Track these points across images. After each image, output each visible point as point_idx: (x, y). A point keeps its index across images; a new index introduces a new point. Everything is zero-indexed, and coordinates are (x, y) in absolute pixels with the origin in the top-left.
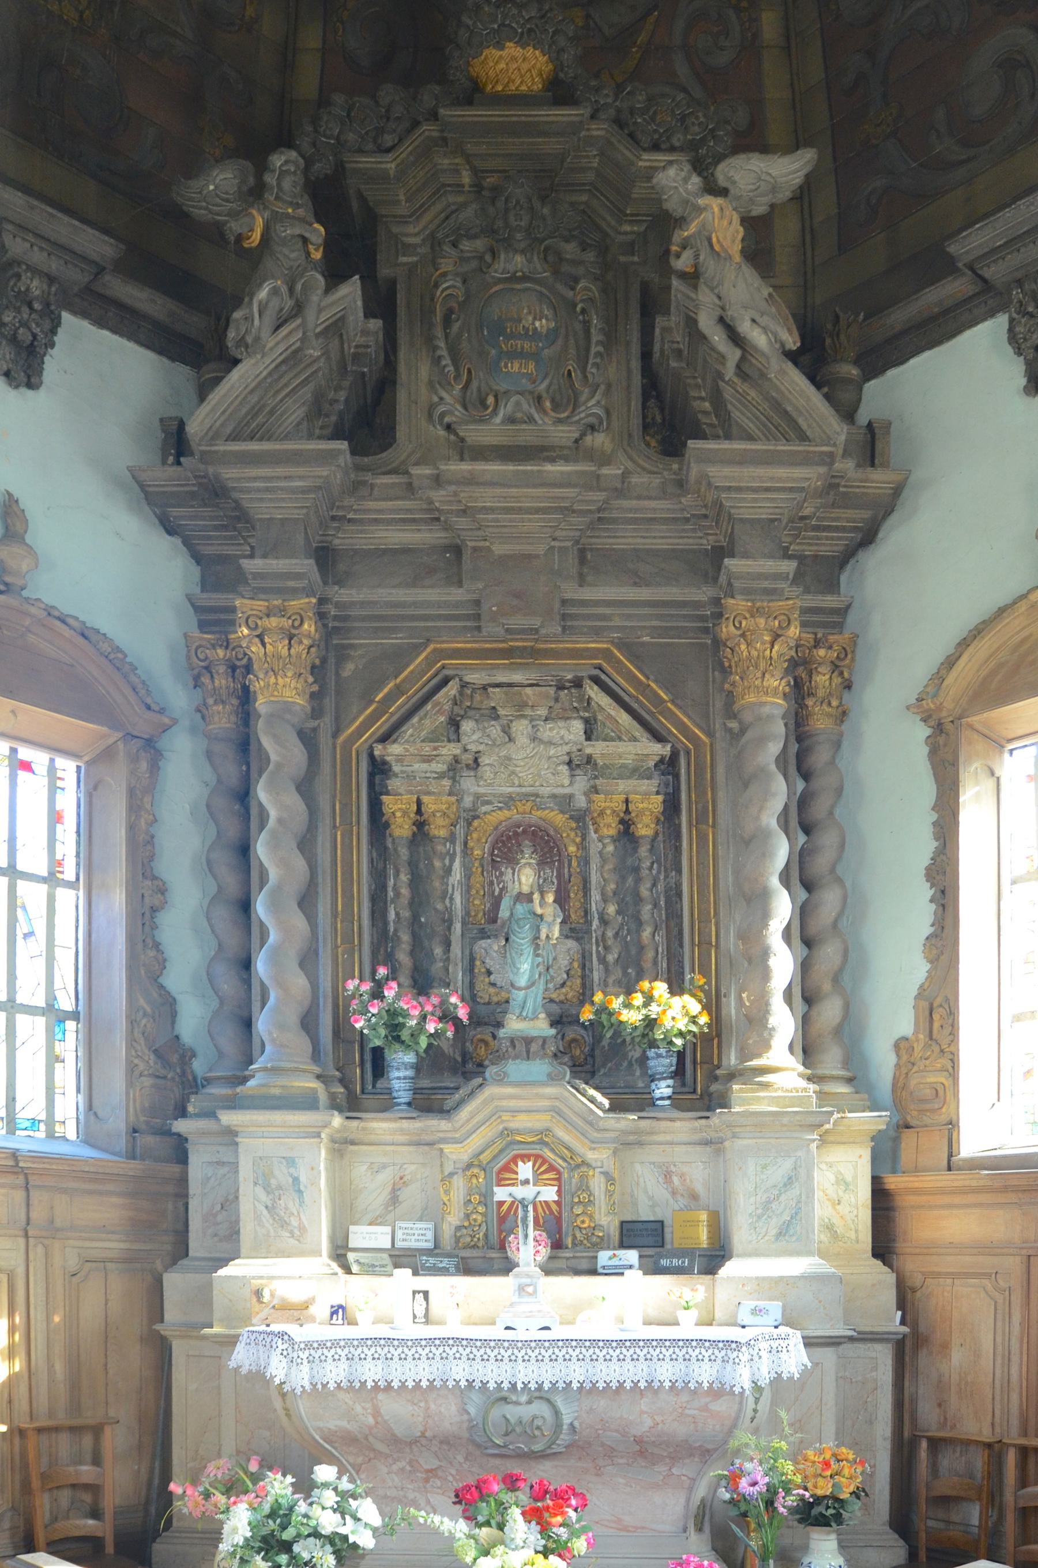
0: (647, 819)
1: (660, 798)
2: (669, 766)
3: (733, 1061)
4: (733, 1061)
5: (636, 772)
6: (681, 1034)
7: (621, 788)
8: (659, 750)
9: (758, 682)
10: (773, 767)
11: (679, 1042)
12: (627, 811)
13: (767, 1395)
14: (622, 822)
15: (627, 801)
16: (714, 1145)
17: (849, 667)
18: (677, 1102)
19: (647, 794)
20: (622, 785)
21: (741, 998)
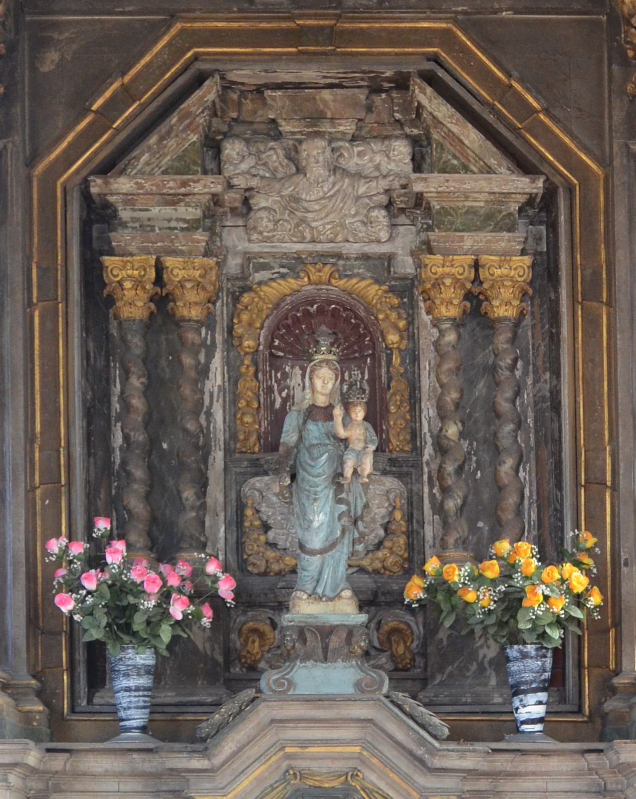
0: (506, 293)
1: (527, 260)
2: (542, 208)
5: (492, 219)
8: (525, 186)
12: (477, 280)
15: (476, 265)
19: (505, 254)
20: (470, 240)
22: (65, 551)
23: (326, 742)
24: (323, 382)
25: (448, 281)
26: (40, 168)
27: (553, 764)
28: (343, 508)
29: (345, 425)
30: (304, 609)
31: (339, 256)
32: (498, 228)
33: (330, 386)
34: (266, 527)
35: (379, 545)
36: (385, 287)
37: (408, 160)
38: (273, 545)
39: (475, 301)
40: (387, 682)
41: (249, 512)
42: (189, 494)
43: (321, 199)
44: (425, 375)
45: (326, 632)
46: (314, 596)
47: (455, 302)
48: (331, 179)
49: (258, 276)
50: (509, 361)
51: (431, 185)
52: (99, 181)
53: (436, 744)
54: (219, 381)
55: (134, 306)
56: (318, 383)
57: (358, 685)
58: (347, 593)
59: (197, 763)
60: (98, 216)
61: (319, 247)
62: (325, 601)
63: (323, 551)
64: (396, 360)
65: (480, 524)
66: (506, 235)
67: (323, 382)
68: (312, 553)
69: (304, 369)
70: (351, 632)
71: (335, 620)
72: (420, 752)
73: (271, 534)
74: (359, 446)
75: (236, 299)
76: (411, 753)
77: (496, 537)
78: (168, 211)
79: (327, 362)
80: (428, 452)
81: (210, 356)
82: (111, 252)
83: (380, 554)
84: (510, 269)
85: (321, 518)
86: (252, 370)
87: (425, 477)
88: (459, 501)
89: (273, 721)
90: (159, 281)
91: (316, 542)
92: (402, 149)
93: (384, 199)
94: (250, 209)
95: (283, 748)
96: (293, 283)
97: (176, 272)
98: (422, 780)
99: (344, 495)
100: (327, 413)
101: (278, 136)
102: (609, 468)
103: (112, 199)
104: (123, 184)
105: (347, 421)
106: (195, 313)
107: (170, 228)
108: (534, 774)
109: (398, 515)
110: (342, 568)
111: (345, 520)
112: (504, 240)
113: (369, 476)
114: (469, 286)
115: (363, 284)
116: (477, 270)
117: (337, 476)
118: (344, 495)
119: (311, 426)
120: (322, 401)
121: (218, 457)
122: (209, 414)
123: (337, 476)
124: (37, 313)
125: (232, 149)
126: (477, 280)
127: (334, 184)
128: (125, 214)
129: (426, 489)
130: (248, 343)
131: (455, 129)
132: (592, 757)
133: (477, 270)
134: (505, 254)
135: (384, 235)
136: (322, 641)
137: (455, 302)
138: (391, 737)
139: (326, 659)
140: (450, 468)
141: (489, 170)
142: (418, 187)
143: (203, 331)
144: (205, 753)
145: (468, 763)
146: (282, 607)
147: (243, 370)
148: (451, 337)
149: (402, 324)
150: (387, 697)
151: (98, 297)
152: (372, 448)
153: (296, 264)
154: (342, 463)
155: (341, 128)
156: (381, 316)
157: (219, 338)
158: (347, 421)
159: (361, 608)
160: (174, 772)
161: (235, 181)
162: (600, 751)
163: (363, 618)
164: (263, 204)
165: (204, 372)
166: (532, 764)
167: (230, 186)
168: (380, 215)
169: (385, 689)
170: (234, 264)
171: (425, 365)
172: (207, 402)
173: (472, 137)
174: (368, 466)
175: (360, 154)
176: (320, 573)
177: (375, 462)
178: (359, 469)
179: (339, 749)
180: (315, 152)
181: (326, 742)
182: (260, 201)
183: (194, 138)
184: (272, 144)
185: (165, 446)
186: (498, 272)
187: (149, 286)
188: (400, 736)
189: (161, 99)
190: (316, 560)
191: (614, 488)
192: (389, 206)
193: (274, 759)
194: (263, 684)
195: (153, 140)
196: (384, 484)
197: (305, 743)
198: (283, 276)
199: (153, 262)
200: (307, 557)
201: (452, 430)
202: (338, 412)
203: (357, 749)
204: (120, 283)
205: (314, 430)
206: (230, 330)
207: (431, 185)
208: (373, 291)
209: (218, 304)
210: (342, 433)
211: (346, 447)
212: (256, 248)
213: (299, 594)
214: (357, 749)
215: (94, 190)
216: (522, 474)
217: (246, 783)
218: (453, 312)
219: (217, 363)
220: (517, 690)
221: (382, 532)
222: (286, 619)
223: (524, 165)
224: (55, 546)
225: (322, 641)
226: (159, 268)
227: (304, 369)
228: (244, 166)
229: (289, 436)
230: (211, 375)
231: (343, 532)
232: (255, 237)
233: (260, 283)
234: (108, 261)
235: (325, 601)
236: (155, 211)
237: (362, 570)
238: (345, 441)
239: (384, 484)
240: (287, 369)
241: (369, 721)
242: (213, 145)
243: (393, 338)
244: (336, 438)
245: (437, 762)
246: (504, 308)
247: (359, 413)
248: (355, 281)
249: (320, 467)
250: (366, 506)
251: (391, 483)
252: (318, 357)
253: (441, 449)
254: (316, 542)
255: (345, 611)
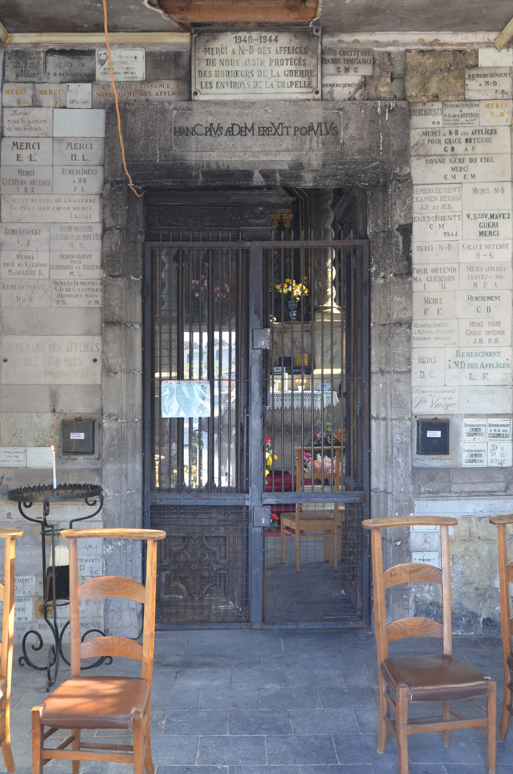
0: (288, 222)
1: (292, 215)
2: (296, 203)
3: (316, 304)
4: (316, 304)
5: (285, 206)
6: (299, 296)
7: (279, 212)
8: (291, 199)
9: (422, 490)
10: (330, 208)
11: (298, 299)
12: (281, 220)
13: (326, 411)
14: (279, 223)
15: (281, 216)
16: (311, 332)
17: (76, 140)
18: (298, 318)
19: (288, 214)
20: (280, 211)
21: (318, 284)
22: (195, 283)
27: (298, 325)
32: (286, 208)
66: (158, 502)
77: (285, 278)
112: (288, 211)
134: (288, 214)
178: (13, 485)
189: (344, 348)
220: (290, 310)
224: (193, 282)
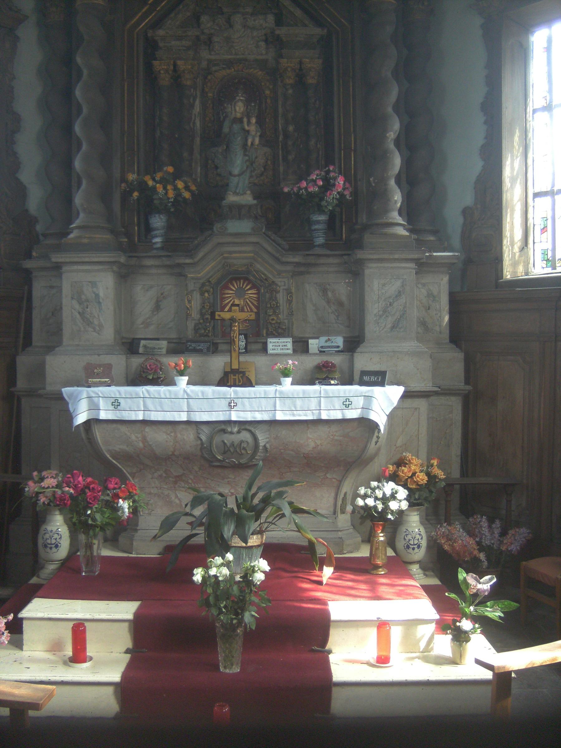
1: (320, 61)
8: (318, 31)
12: (301, 69)
15: (301, 63)
23: (240, 252)
24: (240, 108)
25: (289, 69)
26: (128, 26)
28: (247, 158)
29: (248, 125)
30: (231, 198)
31: (246, 60)
33: (242, 109)
34: (216, 168)
35: (262, 175)
36: (264, 73)
37: (273, 22)
38: (219, 175)
39: (301, 76)
40: (264, 227)
41: (210, 162)
42: (185, 154)
43: (239, 37)
44: (280, 106)
45: (240, 207)
46: (236, 193)
47: (292, 78)
48: (243, 30)
49: (214, 69)
50: (313, 101)
51: (282, 31)
52: (151, 31)
53: (284, 252)
54: (198, 110)
55: (165, 80)
56: (237, 108)
57: (253, 229)
58: (249, 192)
59: (188, 261)
60: (152, 46)
61: (238, 57)
62: (240, 196)
63: (239, 175)
64: (269, 101)
65: (302, 166)
67: (240, 108)
68: (235, 176)
69: (231, 105)
70: (250, 207)
71: (243, 203)
72: (277, 255)
73: (219, 170)
74: (253, 133)
75: (206, 78)
76: (273, 256)
78: (178, 43)
79: (241, 100)
80: (281, 138)
81: (195, 99)
82: (156, 59)
83: (262, 178)
84: (313, 63)
85: (238, 163)
86: (211, 105)
87: (280, 147)
88: (293, 156)
89: (219, 244)
90: (175, 70)
91: (236, 171)
92: (271, 18)
93: (264, 38)
94: (211, 42)
95: (222, 255)
96: (228, 71)
97: (181, 66)
98: (278, 267)
99: (247, 153)
100: (241, 121)
101: (223, 14)
102: (353, 142)
103: (156, 38)
104: (161, 32)
105: (249, 123)
106: (189, 83)
107: (180, 50)
108: (323, 264)
109: (269, 162)
110: (247, 182)
111: (248, 163)
113: (257, 145)
114: (297, 71)
115: (255, 71)
116: (301, 65)
117: (245, 146)
118: (247, 153)
119: (234, 126)
120: (239, 115)
121: (198, 140)
122: (194, 123)
123: (245, 146)
124: (126, 84)
125: (204, 19)
126: (301, 69)
127: (244, 32)
128: (161, 44)
129: (280, 152)
130: (210, 95)
131: (292, 10)
132: (345, 257)
133: (301, 65)
135: (264, 52)
136: (239, 211)
137: (292, 78)
138: (265, 249)
139: (240, 218)
140: (290, 143)
141: (305, 26)
142: (277, 32)
143: (192, 90)
144: (191, 257)
145: (296, 260)
146: (223, 199)
147: (208, 105)
148: (290, 91)
149: (271, 87)
150: (264, 233)
151: (151, 77)
152: (259, 134)
153: (229, 64)
154: (246, 140)
155: (247, 10)
156: (263, 84)
157: (198, 94)
158: (249, 123)
159: (254, 199)
160: (179, 265)
161: (205, 31)
162: (349, 255)
163: (255, 202)
164: (216, 40)
165: (192, 106)
166: (322, 261)
167: (203, 33)
168: (262, 44)
169: (263, 231)
170: (204, 64)
171: (280, 103)
172: (193, 117)
173: (298, 13)
174: (257, 141)
175: (254, 20)
176: (238, 184)
177: (260, 141)
179: (245, 255)
180: (238, 19)
181: (240, 252)
182: (216, 39)
183: (188, 14)
184: (219, 16)
185: (177, 136)
186: (309, 66)
187: (170, 72)
188: (269, 249)
190: (236, 179)
191: (355, 151)
192: (266, 41)
193: (219, 259)
194: (215, 229)
195: (172, 15)
196: (465, 578)
197: (230, 253)
198: (224, 68)
199: (172, 63)
200: (233, 178)
201: (291, 128)
202: (245, 120)
203: (252, 255)
204: (159, 71)
205: (236, 127)
206: (203, 90)
207: (282, 31)
208: (260, 74)
209: (198, 80)
210: (247, 128)
211: (249, 134)
212: (213, 57)
213: (229, 192)
214: (252, 255)
215: (149, 35)
216: (319, 146)
217: (208, 269)
218: (291, 81)
219: (197, 102)
221: (263, 169)
222: (224, 203)
223: (319, 23)
225: (239, 211)
226: (175, 65)
227: (231, 105)
228: (209, 25)
229: (226, 130)
230: (195, 108)
231: (247, 167)
232: (213, 53)
233: (216, 71)
234: (156, 63)
235: (240, 196)
236: (173, 43)
237: (255, 184)
238: (248, 132)
239: (465, 578)
240: (225, 105)
241: (257, 243)
242: (197, 18)
243: (267, 92)
244: (244, 129)
245: (284, 259)
246: (311, 80)
247: (254, 120)
248: (252, 70)
249: (238, 140)
250: (256, 158)
251: (267, 150)
252: (238, 98)
253: (286, 136)
254: (236, 171)
255: (248, 199)
